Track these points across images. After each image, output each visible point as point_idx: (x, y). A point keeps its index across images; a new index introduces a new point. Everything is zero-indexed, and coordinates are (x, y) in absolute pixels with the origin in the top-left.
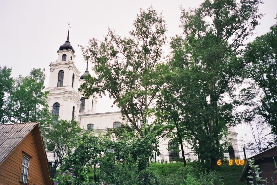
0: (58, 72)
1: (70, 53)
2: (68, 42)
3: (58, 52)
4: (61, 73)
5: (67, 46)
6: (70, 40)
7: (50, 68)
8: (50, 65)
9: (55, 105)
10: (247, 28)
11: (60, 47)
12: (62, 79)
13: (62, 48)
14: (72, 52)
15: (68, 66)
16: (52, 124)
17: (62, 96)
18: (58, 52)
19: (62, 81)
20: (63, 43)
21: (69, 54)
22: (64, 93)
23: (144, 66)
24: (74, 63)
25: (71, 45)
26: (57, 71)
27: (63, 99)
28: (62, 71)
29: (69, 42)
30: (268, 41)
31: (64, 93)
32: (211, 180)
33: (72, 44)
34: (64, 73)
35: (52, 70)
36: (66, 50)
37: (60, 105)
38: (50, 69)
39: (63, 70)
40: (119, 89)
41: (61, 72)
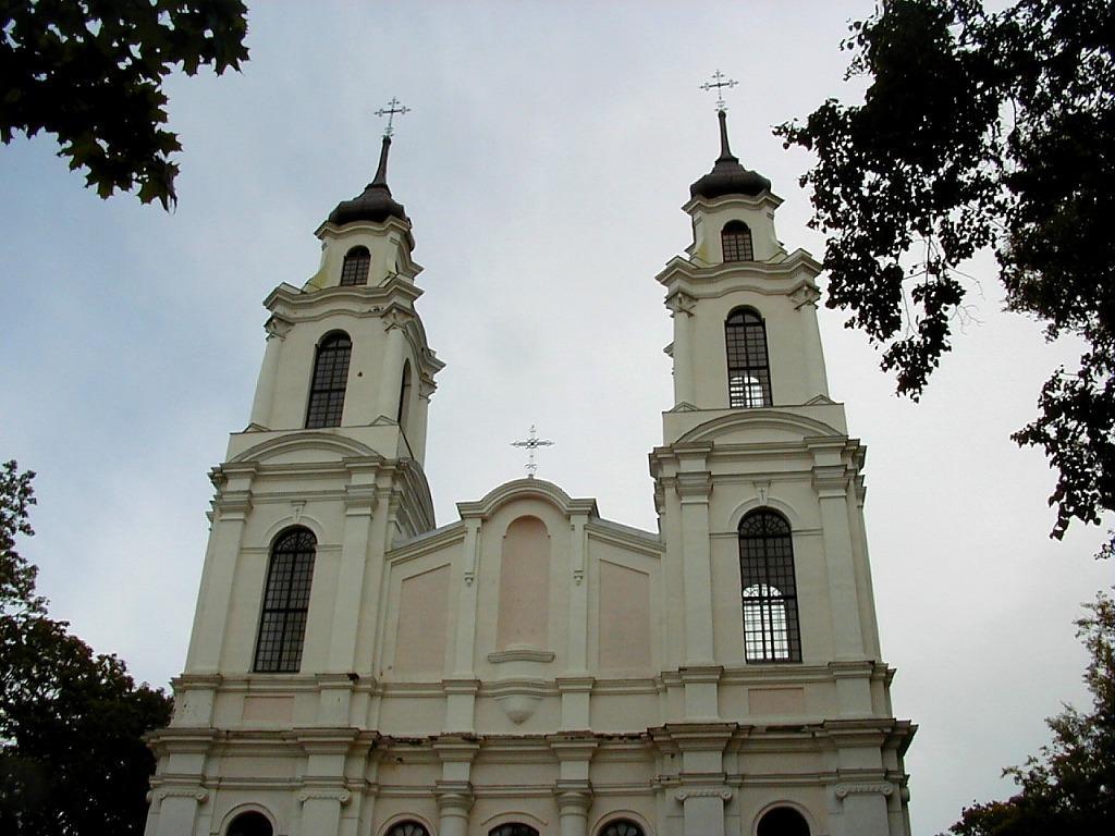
0: (316, 339)
2: (379, 185)
3: (321, 233)
4: (334, 346)
8: (270, 302)
9: (288, 544)
10: (389, 129)
12: (334, 387)
15: (788, 285)
17: (339, 485)
18: (321, 233)
19: (334, 395)
26: (308, 337)
35: (686, 304)
41: (738, 319)
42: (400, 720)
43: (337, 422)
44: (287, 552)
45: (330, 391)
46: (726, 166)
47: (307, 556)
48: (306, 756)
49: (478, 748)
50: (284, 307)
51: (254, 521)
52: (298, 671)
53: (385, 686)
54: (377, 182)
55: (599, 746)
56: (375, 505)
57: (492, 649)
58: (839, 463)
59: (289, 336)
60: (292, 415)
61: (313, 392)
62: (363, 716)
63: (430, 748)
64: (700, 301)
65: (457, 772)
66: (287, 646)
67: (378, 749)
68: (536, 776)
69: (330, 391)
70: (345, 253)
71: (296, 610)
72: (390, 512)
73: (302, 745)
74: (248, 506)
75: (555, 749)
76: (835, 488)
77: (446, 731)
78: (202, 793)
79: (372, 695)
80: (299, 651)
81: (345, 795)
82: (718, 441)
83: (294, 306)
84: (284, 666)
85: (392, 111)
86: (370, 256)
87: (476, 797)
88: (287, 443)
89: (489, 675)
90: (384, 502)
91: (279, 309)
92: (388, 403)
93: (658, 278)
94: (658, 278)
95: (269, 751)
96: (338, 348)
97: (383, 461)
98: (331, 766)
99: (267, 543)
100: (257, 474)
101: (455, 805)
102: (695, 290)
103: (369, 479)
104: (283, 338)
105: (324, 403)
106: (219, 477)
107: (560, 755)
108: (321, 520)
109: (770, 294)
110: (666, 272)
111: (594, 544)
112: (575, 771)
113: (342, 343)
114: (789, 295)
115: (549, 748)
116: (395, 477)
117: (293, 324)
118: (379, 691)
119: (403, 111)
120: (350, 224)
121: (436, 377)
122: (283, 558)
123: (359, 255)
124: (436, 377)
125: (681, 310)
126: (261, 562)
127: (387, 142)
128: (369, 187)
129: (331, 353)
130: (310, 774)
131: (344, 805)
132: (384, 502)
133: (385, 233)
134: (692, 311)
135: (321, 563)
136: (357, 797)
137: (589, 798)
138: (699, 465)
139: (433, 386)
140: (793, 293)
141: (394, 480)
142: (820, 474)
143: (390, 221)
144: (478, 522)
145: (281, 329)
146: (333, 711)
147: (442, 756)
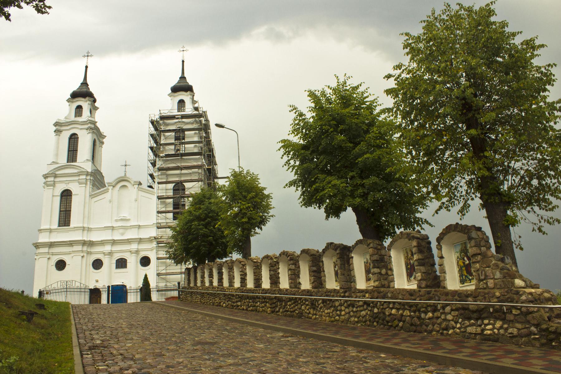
0: (68, 136)
2: (183, 78)
3: (68, 101)
5: (180, 86)
6: (89, 81)
7: (55, 128)
9: (65, 194)
12: (75, 149)
13: (75, 95)
16: (246, 222)
17: (76, 178)
18: (68, 101)
19: (74, 152)
20: (75, 86)
21: (85, 104)
22: (78, 174)
24: (96, 122)
25: (190, 84)
26: (66, 135)
27: (77, 183)
28: (76, 136)
29: (185, 78)
31: (78, 174)
32: (299, 347)
33: (92, 88)
34: (78, 138)
36: (83, 99)
37: (73, 193)
38: (55, 131)
41: (73, 137)
42: (95, 237)
43: (75, 161)
44: (65, 196)
45: (73, 151)
46: (183, 80)
47: (70, 197)
49: (114, 242)
50: (59, 127)
51: (55, 189)
52: (69, 226)
53: (91, 228)
55: (140, 241)
56: (86, 184)
59: (61, 135)
60: (63, 159)
61: (69, 151)
62: (86, 237)
63: (102, 243)
66: (66, 220)
67: (91, 244)
69: (73, 151)
70: (75, 107)
71: (68, 211)
72: (90, 185)
73: (71, 244)
74: (54, 185)
78: (48, 256)
79: (88, 231)
80: (70, 221)
81: (82, 255)
84: (66, 225)
85: (88, 56)
87: (113, 253)
89: (115, 225)
90: (88, 183)
92: (88, 155)
93: (168, 95)
94: (168, 95)
96: (74, 138)
97: (88, 172)
98: (79, 248)
99: (59, 194)
100: (56, 176)
103: (84, 177)
104: (59, 135)
105: (72, 154)
106: (46, 176)
107: (39, 246)
108: (74, 188)
109: (81, 129)
115: (129, 241)
116: (91, 175)
117: (62, 131)
118: (89, 229)
121: (104, 140)
122: (64, 197)
123: (79, 108)
124: (104, 140)
126: (59, 198)
127: (87, 67)
128: (82, 84)
129: (73, 140)
131: (83, 257)
132: (88, 183)
133: (86, 101)
135: (74, 198)
136: (85, 254)
137: (137, 252)
139: (103, 143)
142: (80, 181)
144: (112, 187)
145: (58, 133)
146: (77, 236)
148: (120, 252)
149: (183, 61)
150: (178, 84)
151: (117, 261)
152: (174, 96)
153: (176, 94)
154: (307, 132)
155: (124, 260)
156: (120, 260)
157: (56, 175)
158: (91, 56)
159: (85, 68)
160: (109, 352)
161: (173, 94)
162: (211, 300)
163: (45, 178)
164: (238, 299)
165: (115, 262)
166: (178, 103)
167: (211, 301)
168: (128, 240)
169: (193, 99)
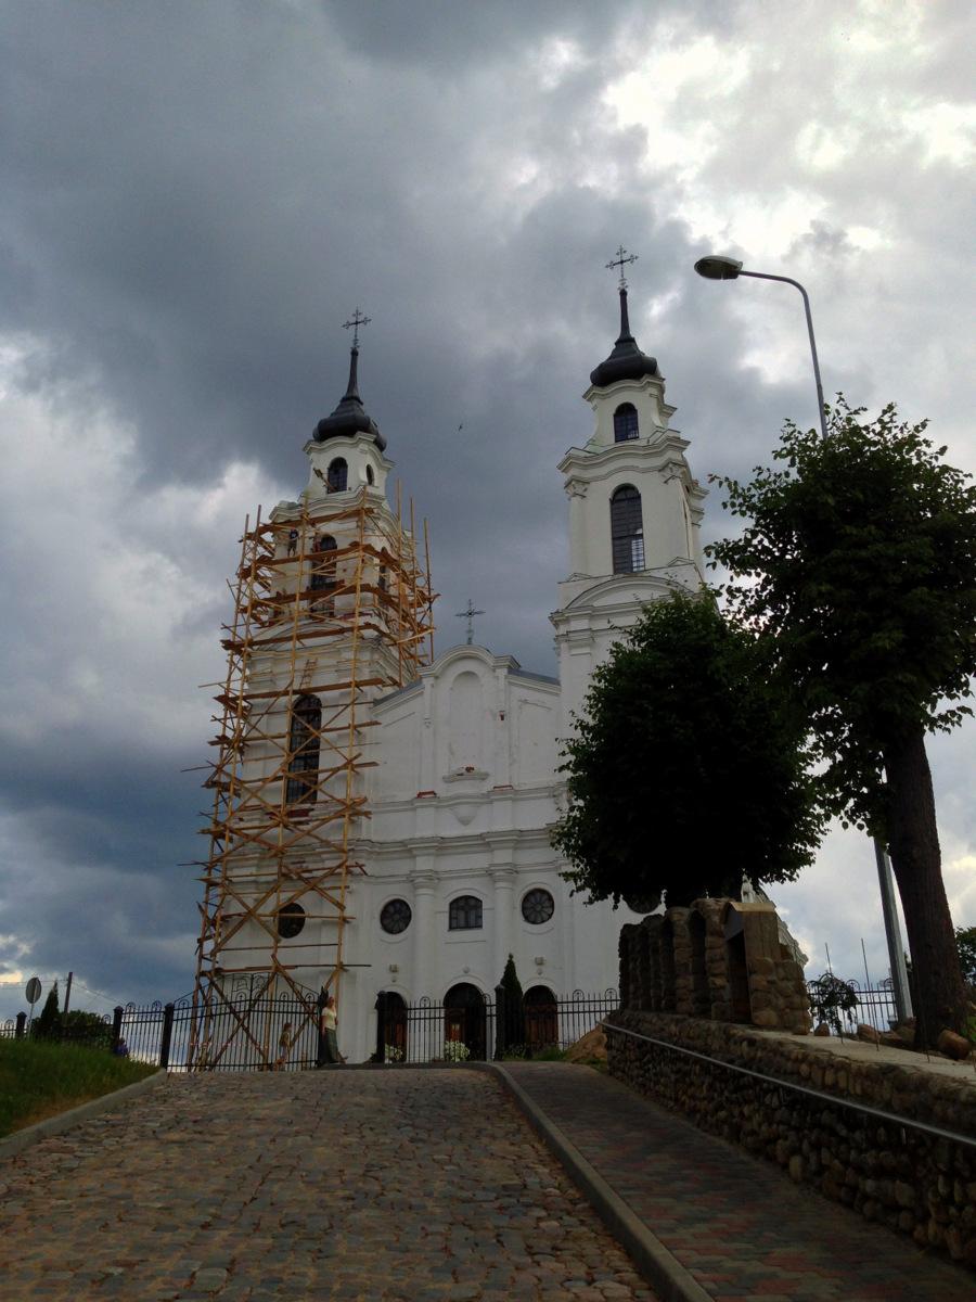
0: (609, 495)
1: (362, 452)
2: (351, 399)
3: (588, 396)
4: (626, 501)
6: (362, 391)
8: (565, 466)
10: (356, 341)
11: (315, 425)
14: (374, 448)
15: (659, 461)
21: (634, 394)
23: (911, 519)
26: (602, 493)
29: (357, 399)
30: (614, 1069)
33: (369, 410)
34: (639, 497)
35: (579, 489)
38: (568, 485)
39: (636, 484)
40: (106, 1142)
48: (415, 857)
54: (350, 395)
57: (445, 772)
58: (586, 627)
64: (593, 484)
65: (424, 863)
68: (481, 861)
70: (614, 412)
75: (488, 843)
76: (582, 646)
77: (418, 835)
82: (596, 604)
83: (586, 467)
86: (636, 411)
88: (600, 588)
91: (574, 472)
95: (476, 849)
101: (503, 880)
102: (587, 474)
107: (415, 852)
110: (565, 462)
111: (514, 689)
112: (503, 856)
113: (630, 494)
114: (660, 471)
115: (485, 842)
119: (365, 321)
120: (614, 384)
123: (339, 466)
125: (575, 495)
130: (496, 862)
134: (585, 494)
138: (583, 624)
140: (662, 469)
141: (372, 653)
143: (646, 379)
147: (415, 852)
148: (462, 875)
149: (354, 354)
150: (334, 417)
151: (451, 904)
152: (604, 397)
153: (608, 390)
154: (781, 545)
155: (472, 902)
156: (462, 903)
157: (595, 609)
158: (348, 325)
159: (350, 356)
160: (377, 1131)
161: (597, 390)
162: (720, 1107)
163: (556, 625)
164: (887, 1158)
165: (447, 908)
166: (615, 416)
167: (722, 1114)
168: (481, 836)
169: (660, 399)
